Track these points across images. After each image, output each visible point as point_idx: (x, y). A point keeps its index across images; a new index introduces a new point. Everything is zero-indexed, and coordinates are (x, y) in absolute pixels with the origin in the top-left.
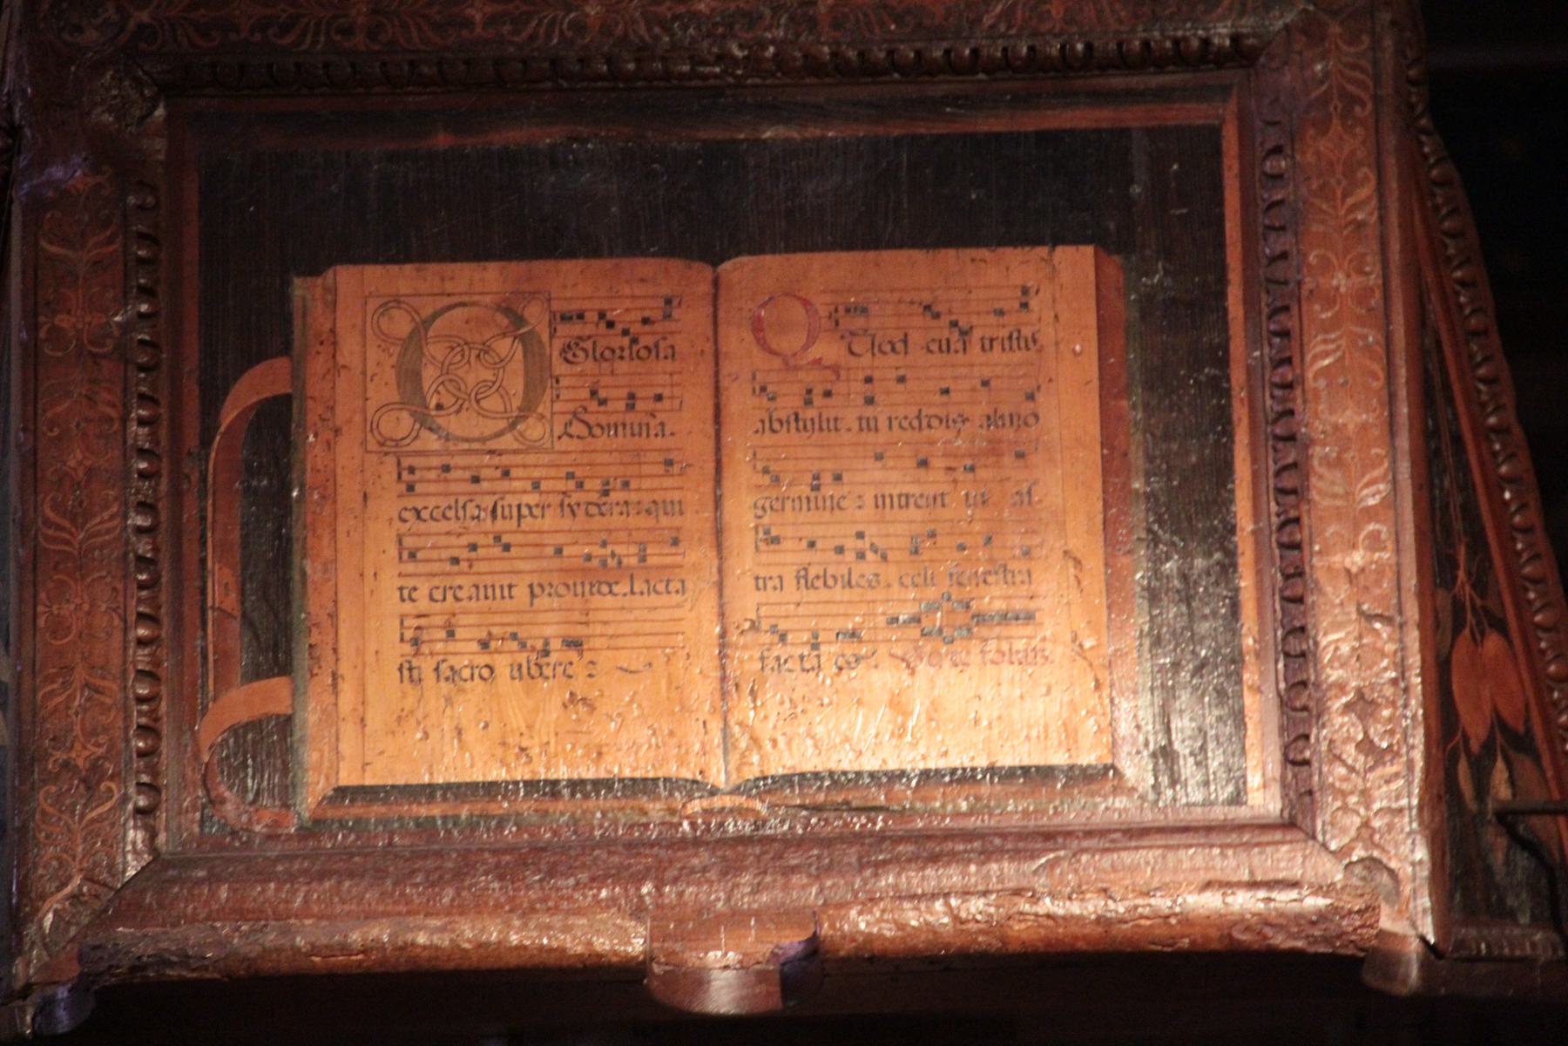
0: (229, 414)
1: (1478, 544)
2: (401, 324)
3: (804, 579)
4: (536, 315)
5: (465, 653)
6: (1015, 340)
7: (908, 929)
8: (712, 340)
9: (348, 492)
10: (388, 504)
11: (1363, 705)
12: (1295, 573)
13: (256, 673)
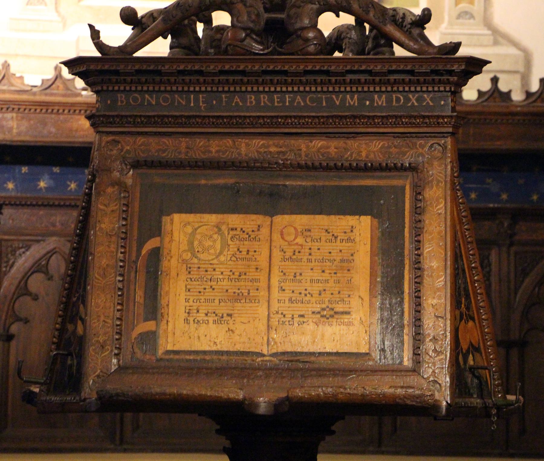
0: (144, 252)
1: (468, 296)
2: (189, 229)
4: (224, 228)
5: (201, 316)
6: (349, 240)
9: (173, 273)
10: (183, 276)
11: (435, 340)
13: (146, 320)
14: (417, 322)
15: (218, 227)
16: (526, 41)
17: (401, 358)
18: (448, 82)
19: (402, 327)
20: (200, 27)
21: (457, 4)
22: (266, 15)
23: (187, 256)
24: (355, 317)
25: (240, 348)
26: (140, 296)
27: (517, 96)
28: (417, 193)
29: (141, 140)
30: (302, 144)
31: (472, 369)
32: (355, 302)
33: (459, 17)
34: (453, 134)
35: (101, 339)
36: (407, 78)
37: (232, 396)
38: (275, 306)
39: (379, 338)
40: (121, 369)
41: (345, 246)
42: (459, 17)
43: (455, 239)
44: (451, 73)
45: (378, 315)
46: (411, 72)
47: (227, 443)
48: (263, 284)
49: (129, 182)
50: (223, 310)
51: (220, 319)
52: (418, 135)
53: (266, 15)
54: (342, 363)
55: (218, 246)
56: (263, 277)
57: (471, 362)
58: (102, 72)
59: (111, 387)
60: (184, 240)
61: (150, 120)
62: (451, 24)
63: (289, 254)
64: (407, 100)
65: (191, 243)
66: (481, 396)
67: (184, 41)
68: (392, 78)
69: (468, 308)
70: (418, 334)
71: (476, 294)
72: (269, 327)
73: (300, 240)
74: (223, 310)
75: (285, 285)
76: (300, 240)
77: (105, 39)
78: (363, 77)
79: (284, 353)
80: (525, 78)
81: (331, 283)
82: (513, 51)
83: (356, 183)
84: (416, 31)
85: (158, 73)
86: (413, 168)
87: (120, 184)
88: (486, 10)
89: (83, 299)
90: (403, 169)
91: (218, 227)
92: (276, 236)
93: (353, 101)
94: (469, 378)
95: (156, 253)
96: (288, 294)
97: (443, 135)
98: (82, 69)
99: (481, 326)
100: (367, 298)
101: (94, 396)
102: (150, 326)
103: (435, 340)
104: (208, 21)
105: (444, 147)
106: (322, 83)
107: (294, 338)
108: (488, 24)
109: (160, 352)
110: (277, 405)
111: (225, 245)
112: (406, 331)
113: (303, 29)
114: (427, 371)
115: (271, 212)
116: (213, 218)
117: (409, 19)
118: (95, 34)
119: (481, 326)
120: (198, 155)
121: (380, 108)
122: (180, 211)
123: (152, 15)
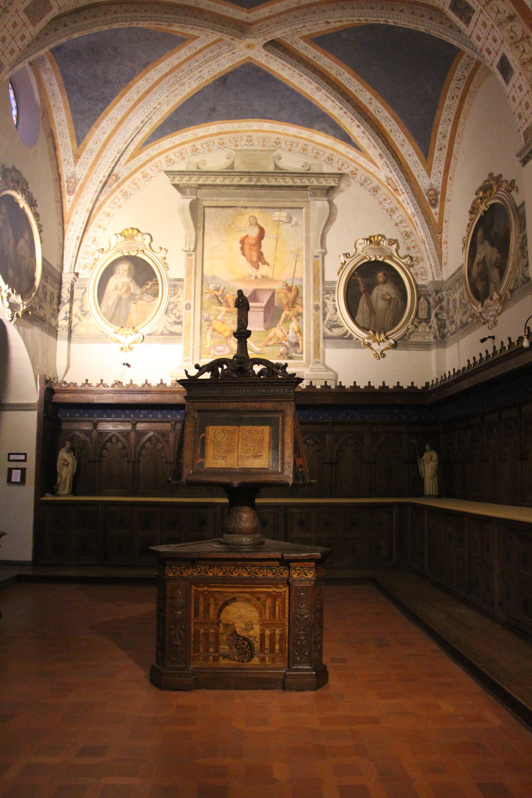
0: (200, 438)
1: (299, 451)
2: (214, 431)
3: (244, 452)
4: (225, 430)
5: (217, 457)
6: (263, 433)
7: (261, 34)
8: (140, 94)
9: (209, 444)
10: (212, 445)
11: (288, 463)
12: (283, 453)
13: (201, 458)
14: (283, 458)
15: (223, 430)
16: (336, 370)
17: (278, 470)
18: (292, 385)
19: (278, 460)
20: (220, 369)
21: (315, 359)
22: (238, 366)
23: (213, 439)
24: (264, 457)
25: (229, 467)
26: (199, 451)
27: (333, 387)
28: (283, 420)
29: (199, 404)
30: (248, 404)
31: (300, 473)
32: (264, 453)
33: (315, 363)
34: (294, 401)
35: (187, 464)
36: (280, 384)
37: (226, 481)
38: (240, 454)
39: (271, 464)
40: (193, 473)
41: (261, 435)
42: (315, 363)
43: (295, 433)
44: (293, 382)
45: (271, 457)
46: (281, 382)
47: (228, 496)
48: (236, 447)
49: (196, 417)
50: (224, 455)
51: (223, 458)
52: (284, 401)
53: (238, 366)
54: (262, 471)
55: (223, 435)
56: (236, 445)
57: (300, 470)
58: (187, 384)
59: (190, 479)
60: (212, 434)
61: (202, 398)
62: (313, 365)
63: (244, 437)
64: (280, 390)
65: (214, 435)
66: (303, 480)
67: (215, 374)
68: (275, 384)
69: (299, 453)
70: (283, 462)
71: (302, 449)
72: (238, 460)
73: (248, 434)
74: (224, 455)
75: (243, 448)
76: (248, 434)
77: (190, 374)
78: (266, 384)
79: (242, 468)
80: (336, 381)
81: (257, 447)
82: (332, 373)
83: (264, 416)
84: (283, 370)
85: (205, 384)
86: (282, 411)
87: (193, 417)
88: (324, 360)
89: (182, 452)
90: (279, 411)
91: (223, 430)
92: (240, 433)
93: (264, 391)
94: (299, 475)
95: (204, 438)
96: (243, 451)
97: (291, 401)
98: (182, 383)
99: (303, 460)
100: (267, 451)
101: (185, 482)
102: (202, 460)
103: (288, 463)
104: (222, 367)
105: (291, 405)
106: (254, 386)
107: (246, 463)
108: (324, 365)
109: (205, 468)
110: (240, 484)
111: (225, 435)
112: (279, 461)
113: (248, 370)
114: (286, 473)
115: (239, 425)
116: (221, 427)
117: (281, 366)
118: (186, 372)
119: (303, 460)
120: (216, 408)
121: (263, 393)
122: (211, 425)
123: (204, 366)
